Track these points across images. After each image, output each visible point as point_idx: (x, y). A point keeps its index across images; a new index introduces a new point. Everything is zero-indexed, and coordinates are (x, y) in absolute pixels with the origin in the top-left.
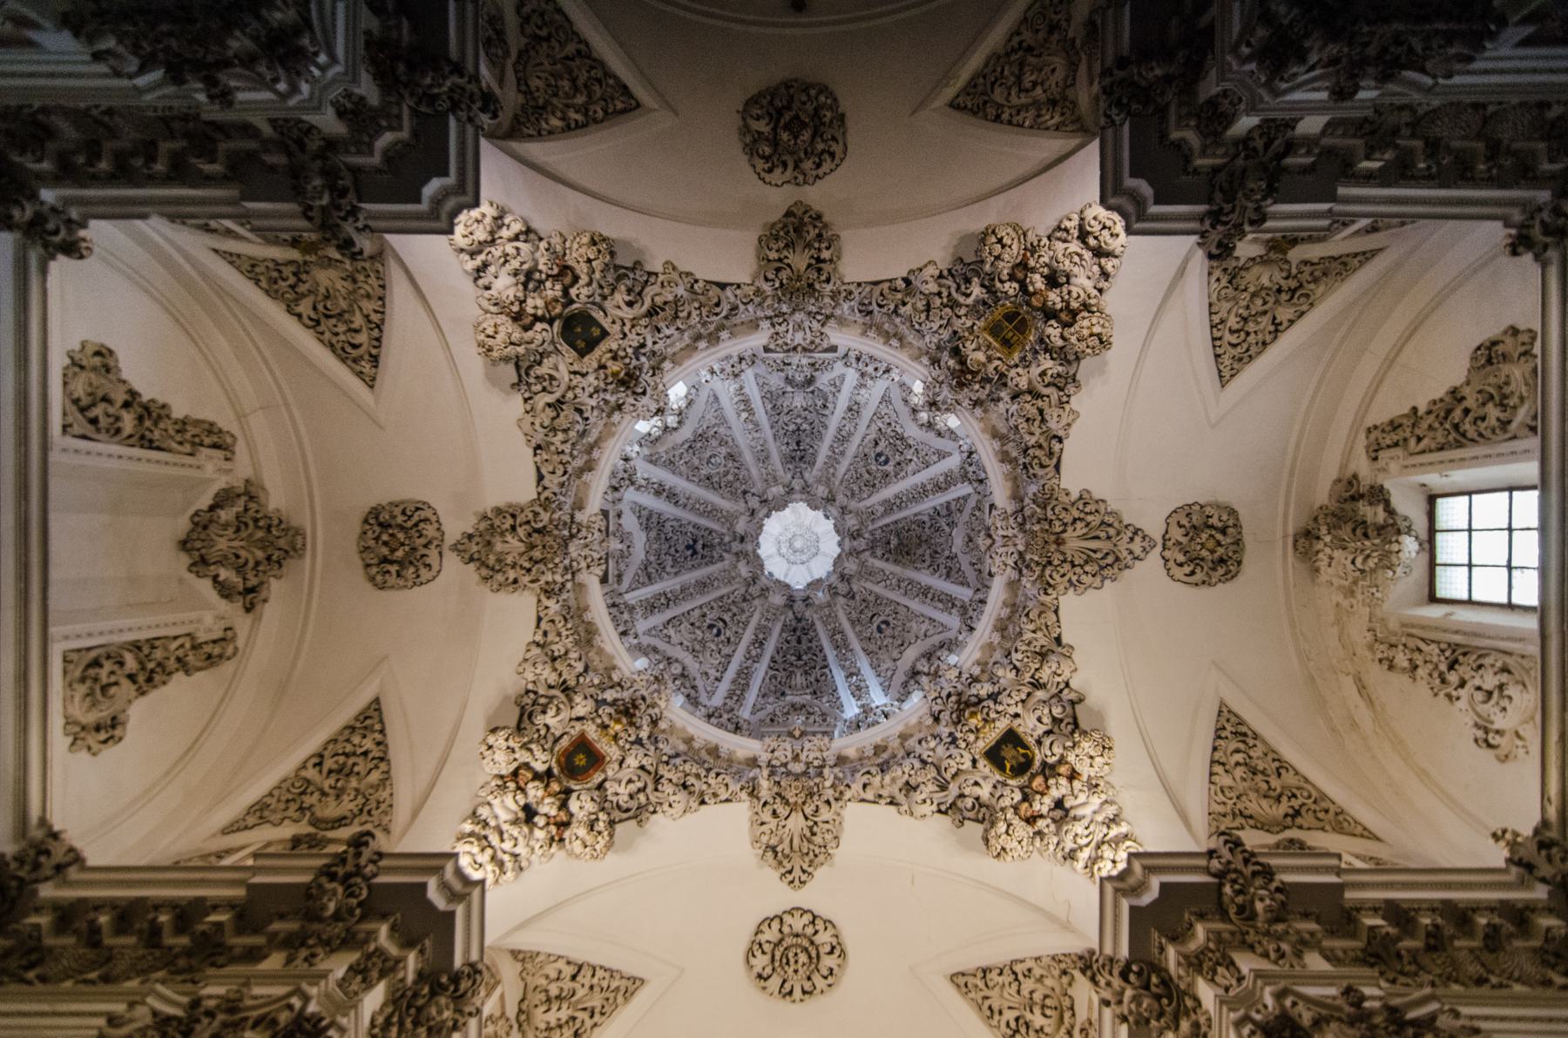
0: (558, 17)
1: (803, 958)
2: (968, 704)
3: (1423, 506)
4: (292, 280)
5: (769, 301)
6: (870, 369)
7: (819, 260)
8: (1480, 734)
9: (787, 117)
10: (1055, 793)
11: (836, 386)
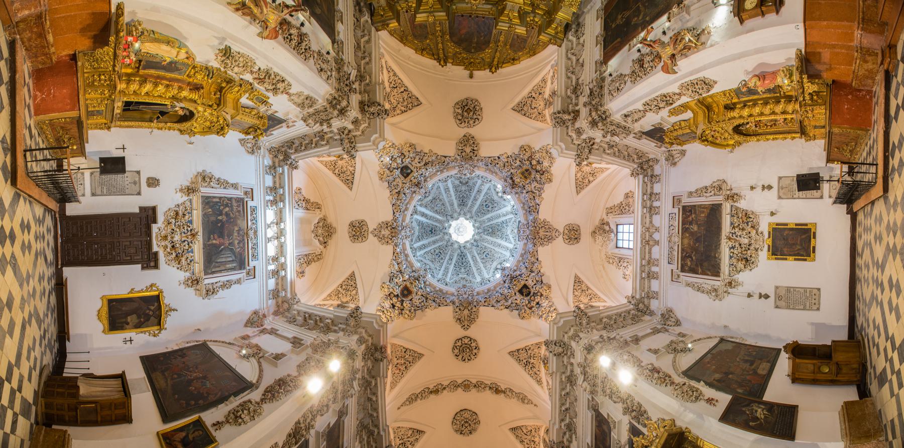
11: (474, 184)
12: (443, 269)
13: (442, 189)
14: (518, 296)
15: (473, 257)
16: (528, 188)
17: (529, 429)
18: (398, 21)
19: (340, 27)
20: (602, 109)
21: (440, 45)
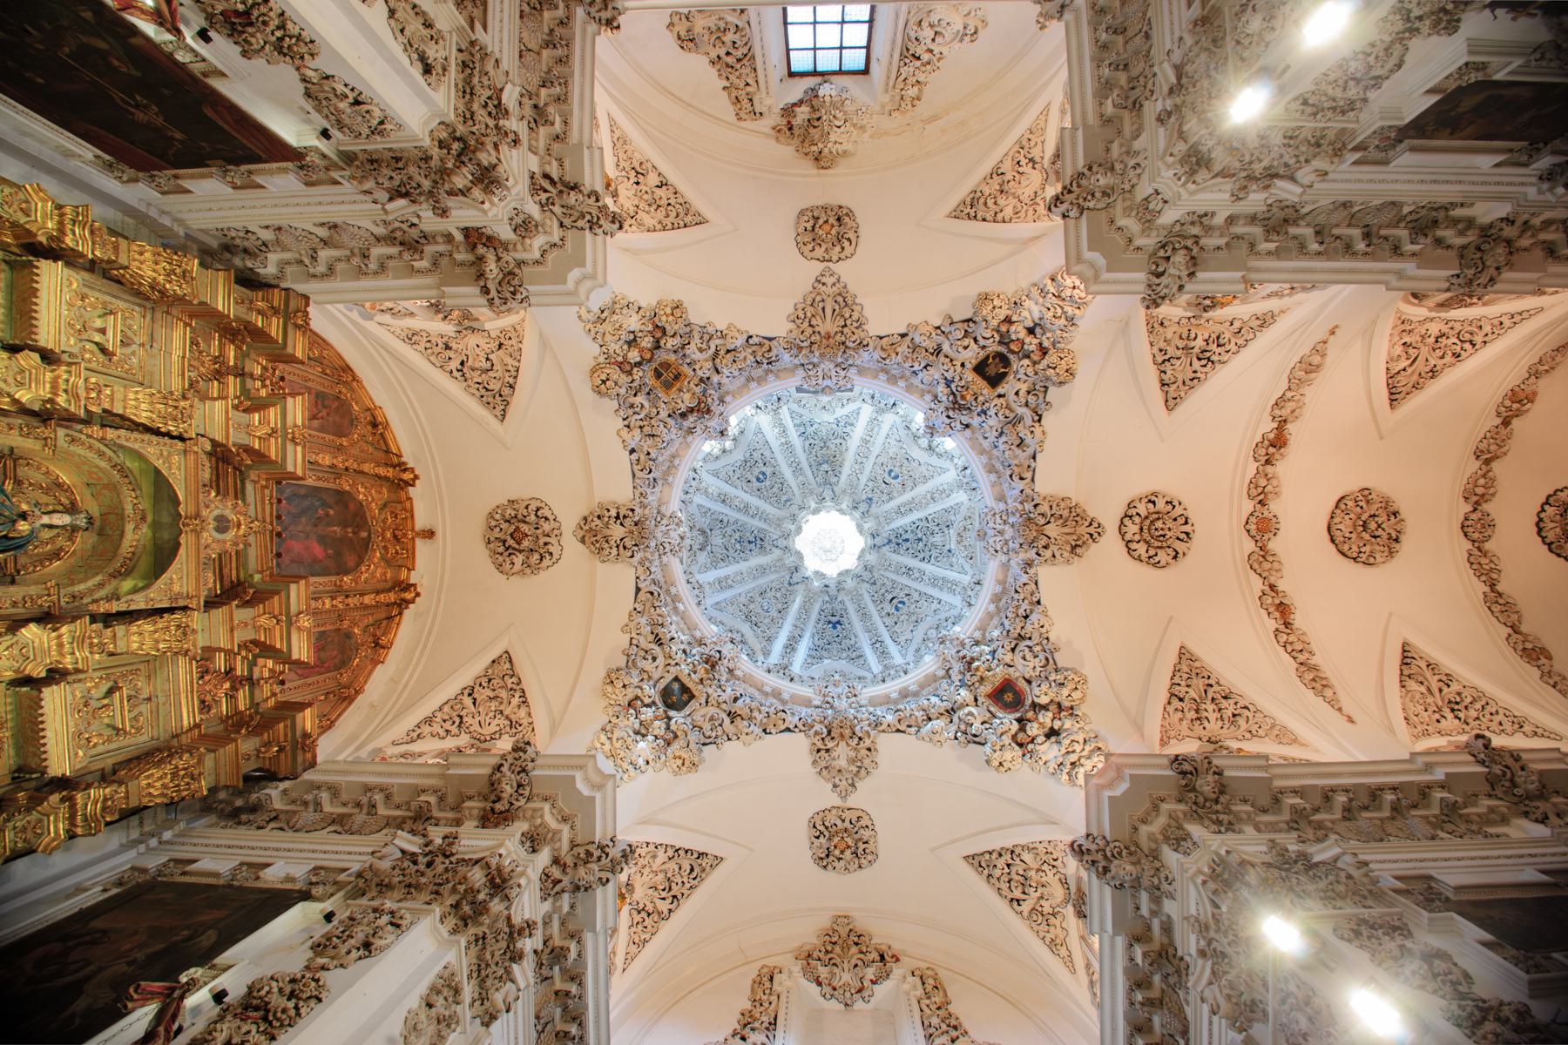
0: (446, 709)
1: (1159, 524)
2: (956, 402)
3: (797, 79)
4: (644, 914)
5: (648, 555)
6: (694, 483)
7: (617, 518)
8: (967, 39)
9: (511, 542)
10: (1022, 334)
11: (706, 512)
12: (935, 592)
13: (720, 597)
14: (1007, 387)
15: (899, 512)
16: (705, 370)
17: (1399, 350)
18: (302, 706)
19: (273, 876)
20: (436, 152)
21: (367, 600)
